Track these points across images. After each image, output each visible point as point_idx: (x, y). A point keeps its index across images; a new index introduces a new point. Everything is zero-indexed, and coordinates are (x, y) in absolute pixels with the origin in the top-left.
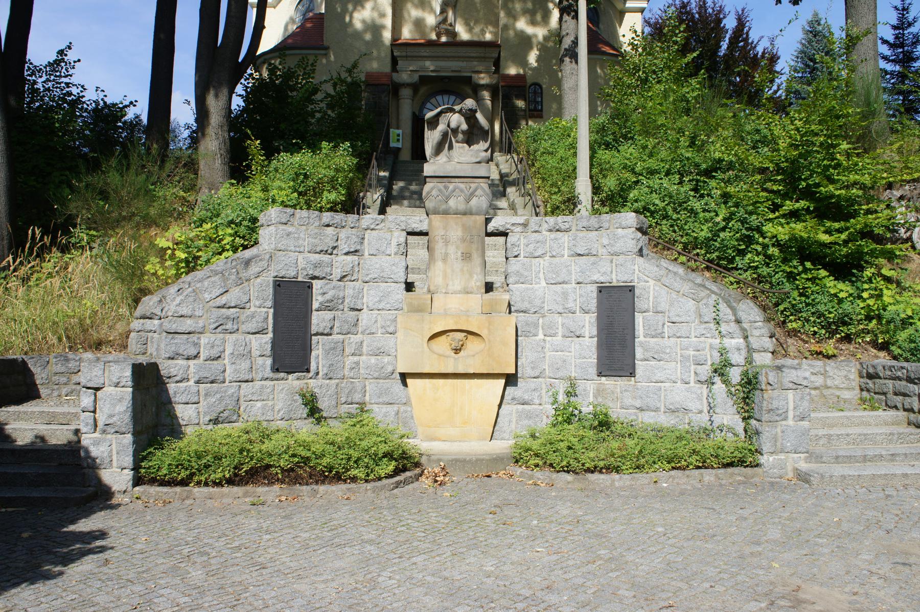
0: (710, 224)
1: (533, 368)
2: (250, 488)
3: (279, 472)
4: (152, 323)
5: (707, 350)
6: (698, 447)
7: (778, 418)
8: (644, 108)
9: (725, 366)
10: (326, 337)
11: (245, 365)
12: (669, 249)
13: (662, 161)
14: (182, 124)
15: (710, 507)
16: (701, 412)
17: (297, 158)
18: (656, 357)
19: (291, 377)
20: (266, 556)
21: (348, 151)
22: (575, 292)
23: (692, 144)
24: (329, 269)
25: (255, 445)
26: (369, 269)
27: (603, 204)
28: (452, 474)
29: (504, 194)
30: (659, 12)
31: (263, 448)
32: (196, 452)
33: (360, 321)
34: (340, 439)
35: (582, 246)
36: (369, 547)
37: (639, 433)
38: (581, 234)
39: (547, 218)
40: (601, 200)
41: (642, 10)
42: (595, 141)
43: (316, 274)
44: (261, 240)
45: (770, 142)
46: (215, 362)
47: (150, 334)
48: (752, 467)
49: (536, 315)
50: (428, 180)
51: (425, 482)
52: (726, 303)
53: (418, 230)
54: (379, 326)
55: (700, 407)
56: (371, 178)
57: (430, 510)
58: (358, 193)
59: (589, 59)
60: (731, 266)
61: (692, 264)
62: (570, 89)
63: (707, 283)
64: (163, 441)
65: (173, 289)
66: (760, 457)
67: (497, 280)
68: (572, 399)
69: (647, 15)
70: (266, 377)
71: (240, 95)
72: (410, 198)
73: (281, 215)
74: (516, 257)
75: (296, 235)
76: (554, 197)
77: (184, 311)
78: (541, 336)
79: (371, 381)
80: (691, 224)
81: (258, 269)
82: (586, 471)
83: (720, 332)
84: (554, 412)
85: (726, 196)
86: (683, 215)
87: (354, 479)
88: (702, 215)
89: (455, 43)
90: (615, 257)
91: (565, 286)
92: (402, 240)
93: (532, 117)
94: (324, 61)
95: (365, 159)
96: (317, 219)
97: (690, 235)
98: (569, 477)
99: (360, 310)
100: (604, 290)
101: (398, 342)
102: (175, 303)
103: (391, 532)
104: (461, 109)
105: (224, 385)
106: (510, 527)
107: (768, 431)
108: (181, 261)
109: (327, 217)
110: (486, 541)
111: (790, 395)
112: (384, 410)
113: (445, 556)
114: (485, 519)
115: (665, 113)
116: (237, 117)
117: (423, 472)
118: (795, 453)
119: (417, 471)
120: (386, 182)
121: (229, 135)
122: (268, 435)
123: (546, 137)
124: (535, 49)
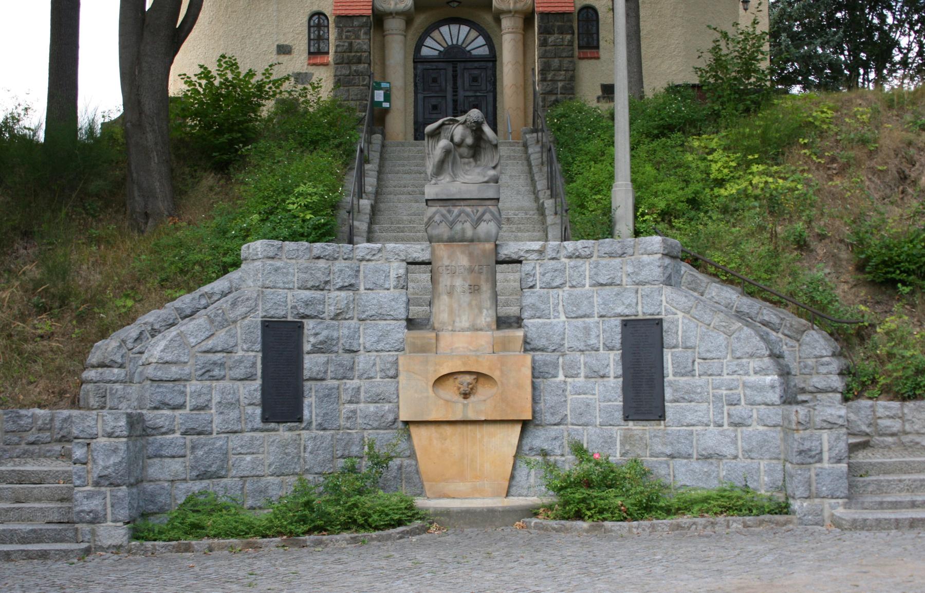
1: (552, 414)
4: (111, 371)
7: (811, 460)
10: (319, 383)
18: (687, 397)
19: (282, 427)
22: (598, 327)
26: (365, 306)
35: (605, 275)
38: (603, 262)
43: (308, 312)
46: (202, 412)
47: (109, 385)
49: (555, 353)
53: (420, 260)
54: (378, 369)
55: (734, 452)
73: (267, 249)
74: (531, 287)
75: (285, 270)
78: (561, 377)
79: (370, 431)
81: (244, 310)
90: (640, 287)
91: (587, 320)
92: (402, 271)
96: (307, 251)
100: (630, 325)
101: (400, 386)
104: (465, 121)
105: (211, 436)
107: (800, 475)
111: (825, 435)
118: (832, 498)
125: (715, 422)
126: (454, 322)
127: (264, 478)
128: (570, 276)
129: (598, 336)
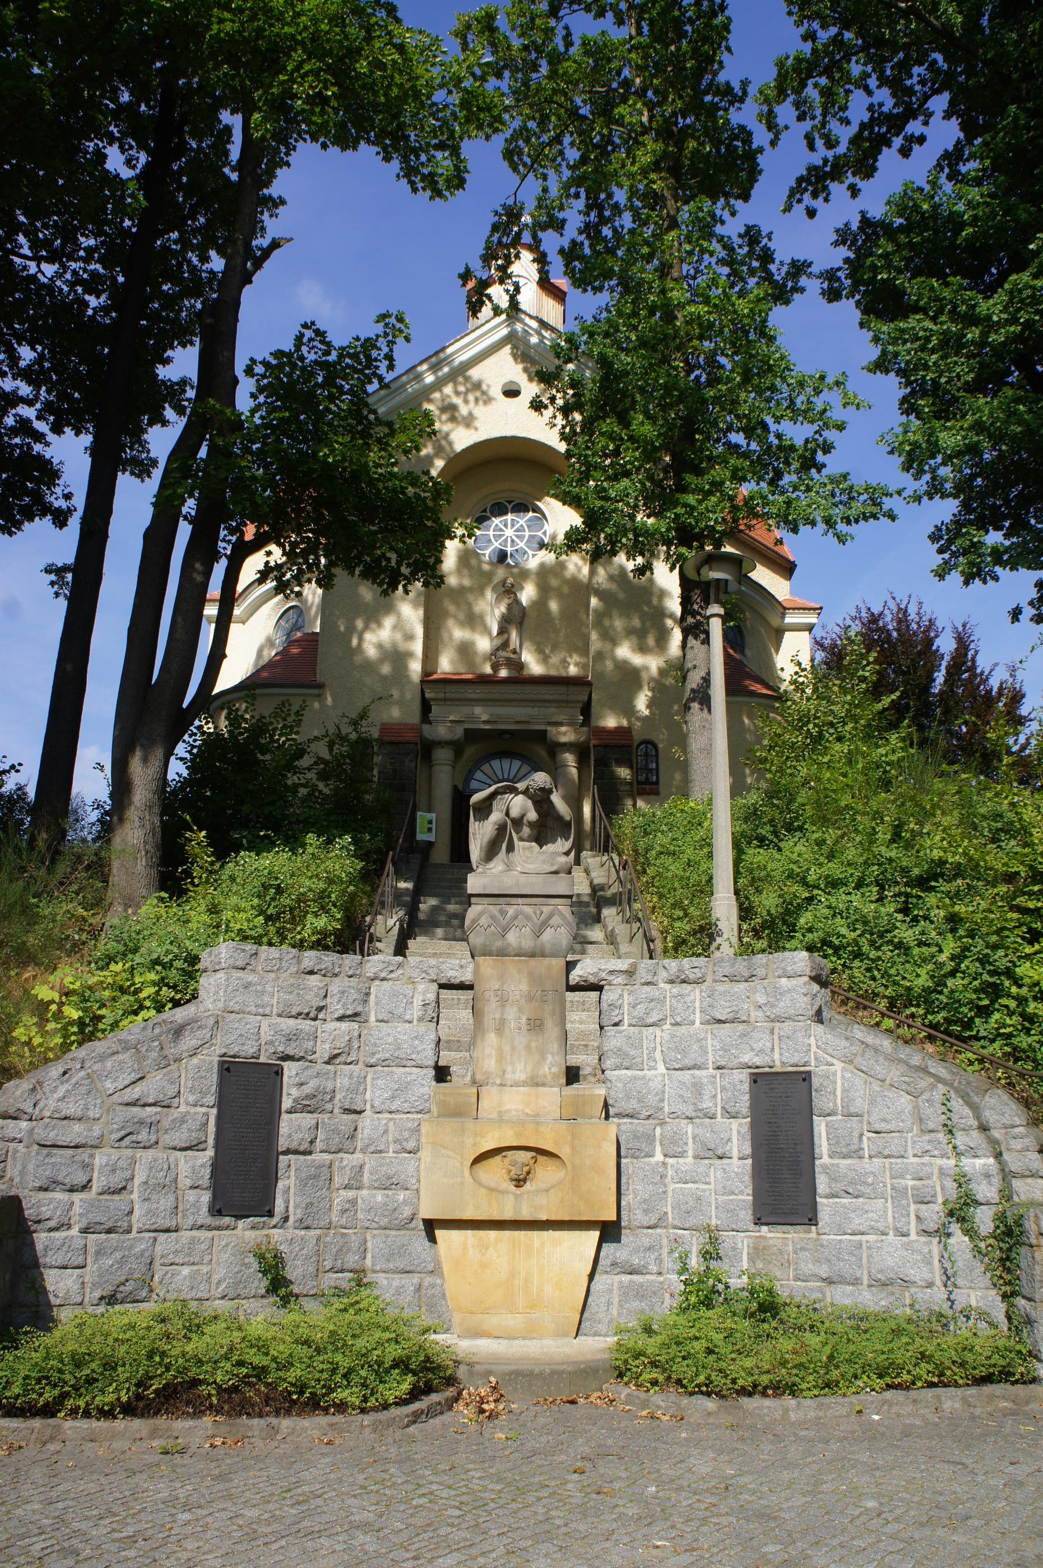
0: (931, 967)
1: (646, 1212)
2: (161, 1421)
3: (214, 1392)
5: (935, 1178)
6: (930, 1348)
8: (818, 780)
9: (966, 1204)
10: (301, 1157)
11: (166, 1202)
12: (865, 1008)
13: (849, 864)
14: (89, 801)
15: (956, 1459)
16: (930, 1285)
17: (266, 861)
19: (241, 1224)
20: (179, 1555)
21: (348, 850)
22: (714, 1083)
23: (896, 836)
24: (311, 1043)
25: (174, 1343)
26: (375, 1045)
27: (757, 934)
28: (510, 1398)
29: (597, 919)
30: (837, 630)
31: (187, 1349)
32: (73, 1355)
33: (359, 1130)
34: (319, 1335)
36: (362, 1538)
37: (827, 1324)
38: (721, 988)
39: (666, 962)
40: (754, 930)
41: (810, 628)
42: (743, 834)
43: (290, 1051)
44: (202, 993)
45: (1018, 832)
46: (116, 1197)
47: (12, 1145)
48: (1024, 1383)
49: (651, 1121)
50: (473, 900)
51: (464, 1412)
52: (962, 1097)
53: (457, 981)
55: (928, 1276)
56: (383, 892)
57: (471, 1466)
58: (364, 917)
59: (728, 703)
60: (968, 1033)
61: (904, 1031)
62: (701, 750)
63: (930, 1063)
64: (18, 1333)
65: (55, 1071)
66: (1038, 1365)
67: (585, 1060)
68: (713, 1264)
69: (818, 633)
70: (199, 1223)
71: (181, 759)
72: (447, 924)
74: (616, 1024)
76: (677, 924)
77: (71, 1109)
78: (659, 1157)
79: (376, 1232)
80: (900, 967)
81: (194, 1043)
82: (738, 1392)
83: (955, 1147)
84: (683, 1287)
85: (954, 920)
86: (887, 950)
87: (341, 1407)
88: (916, 951)
89: (520, 679)
91: (697, 1072)
92: (431, 996)
93: (642, 793)
94: (316, 705)
95: (374, 863)
97: (899, 985)
98: (711, 1404)
99: (360, 1112)
101: (422, 1166)
102: (55, 1096)
103: (402, 1508)
105: (128, 1236)
106: (608, 1499)
108: (71, 1023)
109: (310, 958)
110: (566, 1525)
112: (396, 1283)
113: (494, 1555)
114: (566, 1482)
115: (851, 788)
116: (174, 792)
117: (460, 1394)
119: (451, 1392)
120: (408, 899)
121: (162, 821)
122: (198, 1326)
123: (665, 828)
124: (646, 688)
125: (896, 1229)
126: (504, 1072)
127: (208, 1303)
128: (673, 1009)
129: (715, 1096)
